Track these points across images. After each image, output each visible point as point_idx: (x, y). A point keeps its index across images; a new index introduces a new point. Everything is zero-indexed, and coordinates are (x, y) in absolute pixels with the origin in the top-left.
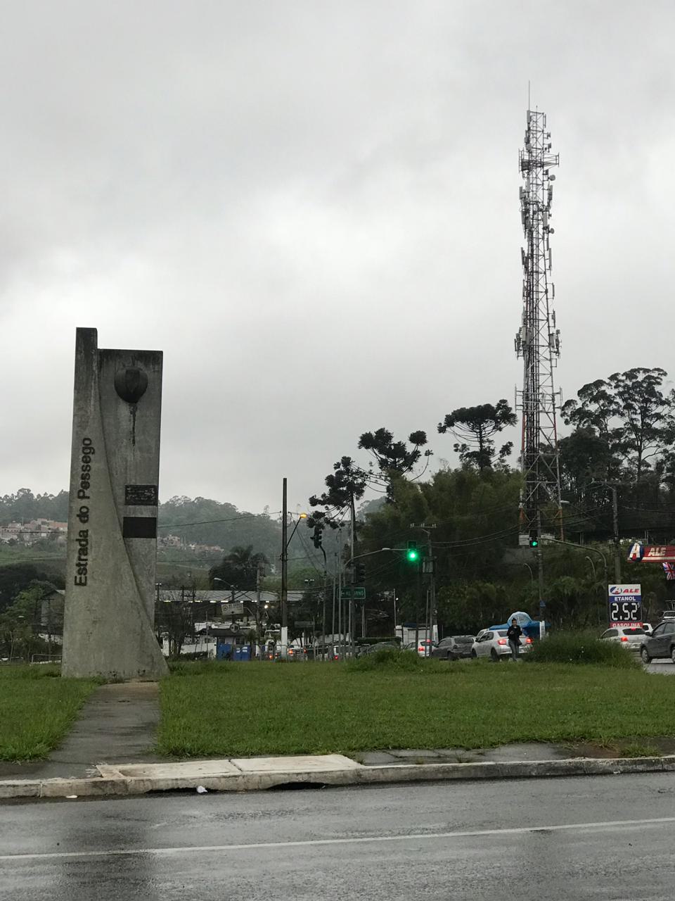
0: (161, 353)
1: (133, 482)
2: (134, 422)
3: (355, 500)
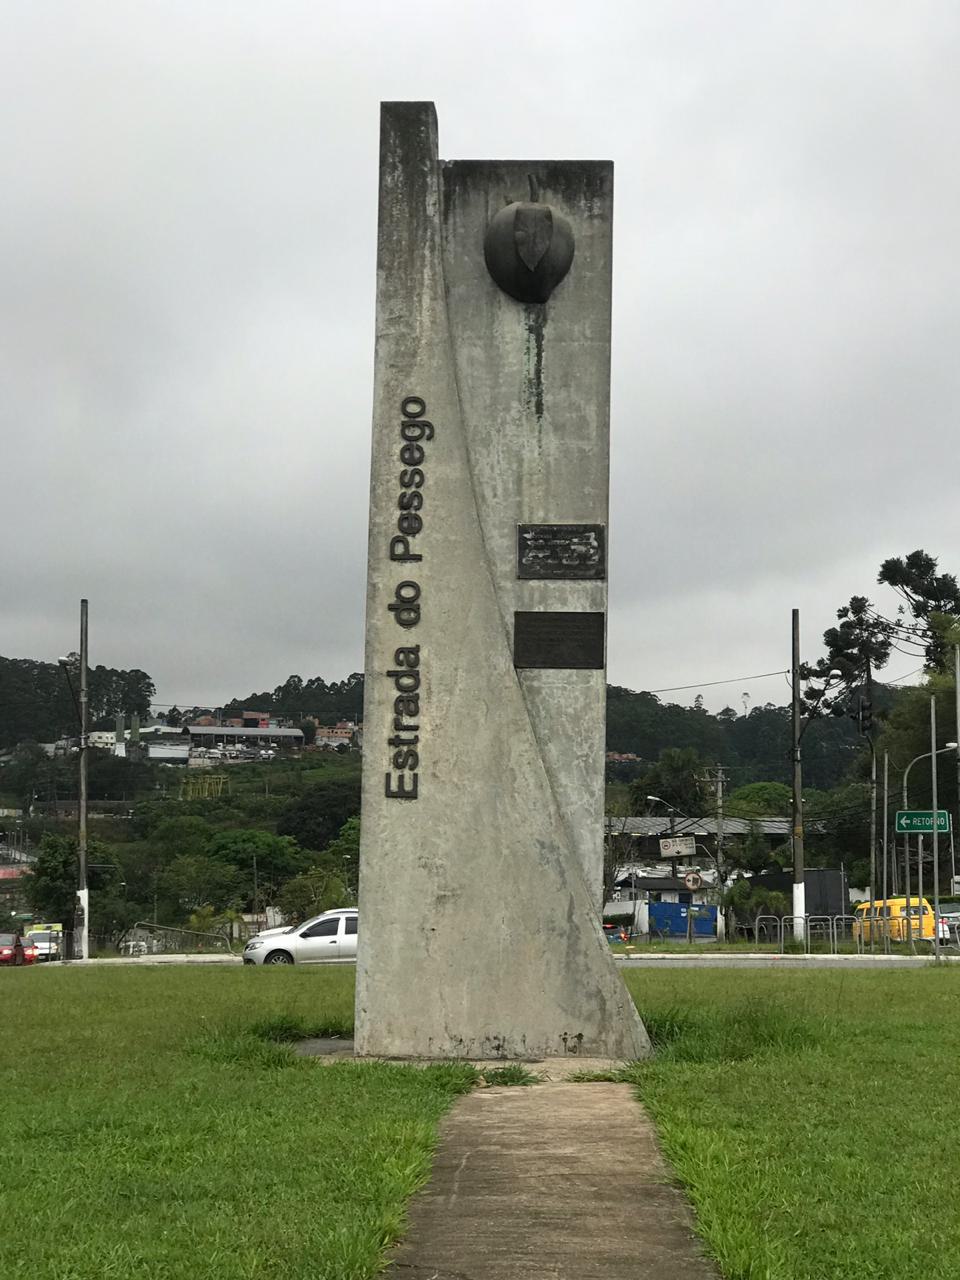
0: (607, 167)
1: (539, 518)
2: (539, 355)
3: (873, 669)
